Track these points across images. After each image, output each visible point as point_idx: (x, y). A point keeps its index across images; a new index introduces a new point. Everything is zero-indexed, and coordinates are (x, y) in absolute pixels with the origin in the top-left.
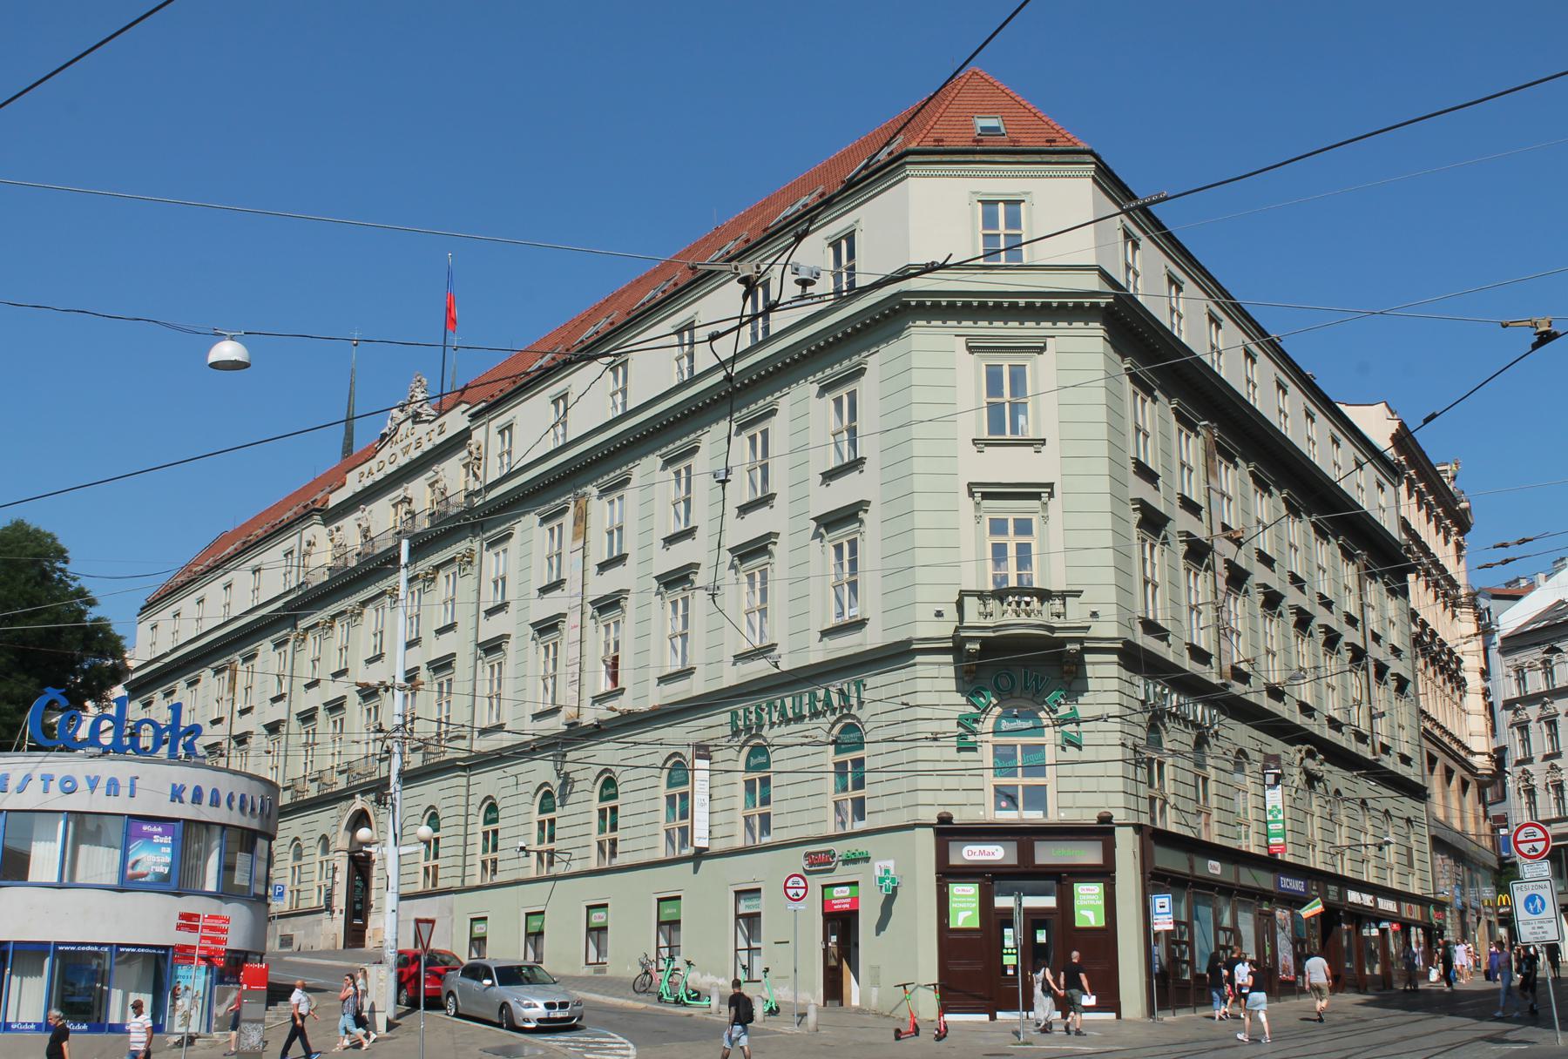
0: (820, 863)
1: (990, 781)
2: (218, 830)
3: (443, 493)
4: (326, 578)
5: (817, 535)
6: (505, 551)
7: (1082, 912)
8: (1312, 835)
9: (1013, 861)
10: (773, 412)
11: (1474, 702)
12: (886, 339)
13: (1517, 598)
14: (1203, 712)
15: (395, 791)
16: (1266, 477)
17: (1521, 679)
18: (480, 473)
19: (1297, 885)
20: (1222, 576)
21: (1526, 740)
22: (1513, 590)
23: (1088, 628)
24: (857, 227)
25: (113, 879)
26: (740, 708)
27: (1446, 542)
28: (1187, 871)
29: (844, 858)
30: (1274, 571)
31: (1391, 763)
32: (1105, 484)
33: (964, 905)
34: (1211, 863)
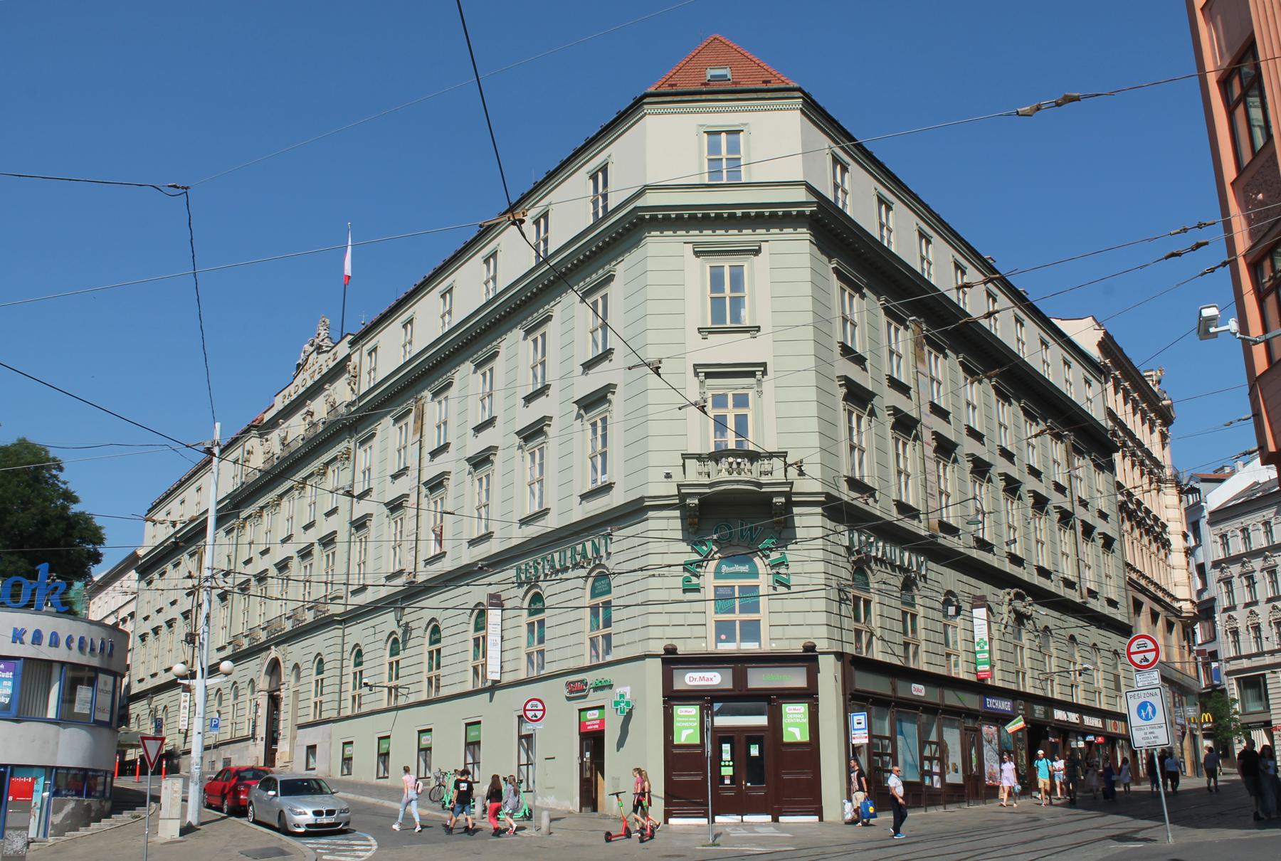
0: (577, 691)
3: (332, 406)
5: (579, 416)
6: (370, 447)
7: (789, 729)
8: (1022, 664)
9: (729, 685)
10: (549, 318)
11: (1177, 558)
12: (629, 250)
13: (1221, 481)
14: (910, 558)
15: (204, 632)
16: (975, 367)
17: (1225, 544)
19: (1004, 705)
20: (929, 445)
21: (1230, 592)
22: (1218, 475)
24: (609, 160)
26: (522, 563)
27: (1152, 431)
28: (890, 693)
29: (594, 686)
30: (983, 444)
31: (1098, 606)
33: (687, 724)
34: (914, 686)
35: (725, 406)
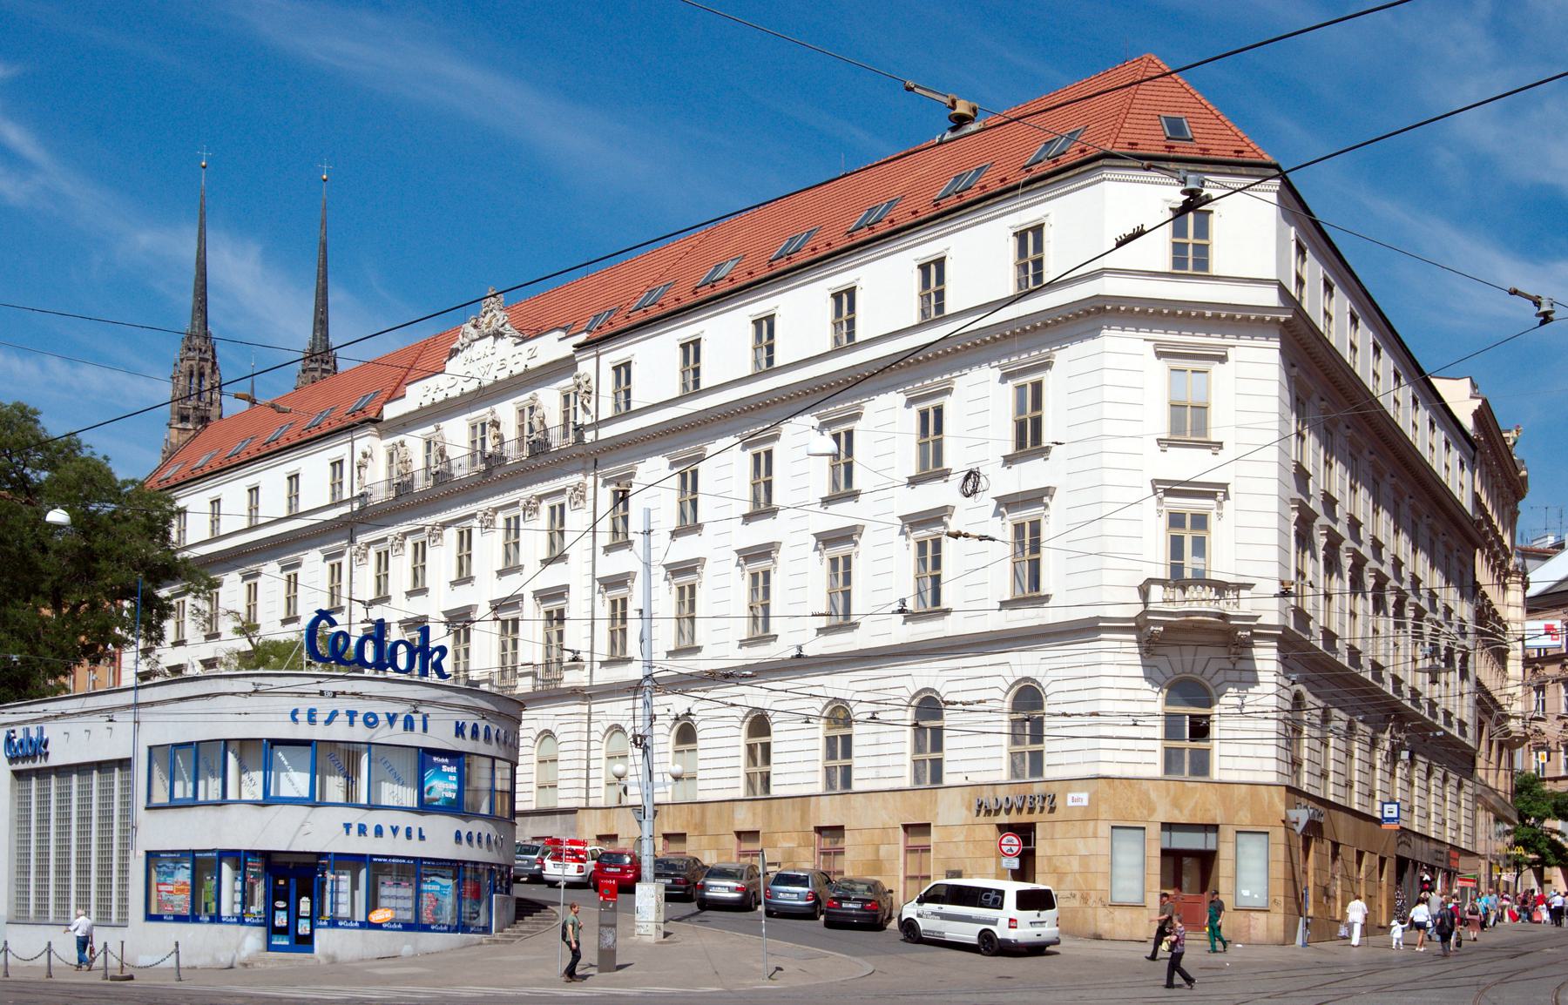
18: (592, 407)
23: (1256, 618)
35: (1183, 526)
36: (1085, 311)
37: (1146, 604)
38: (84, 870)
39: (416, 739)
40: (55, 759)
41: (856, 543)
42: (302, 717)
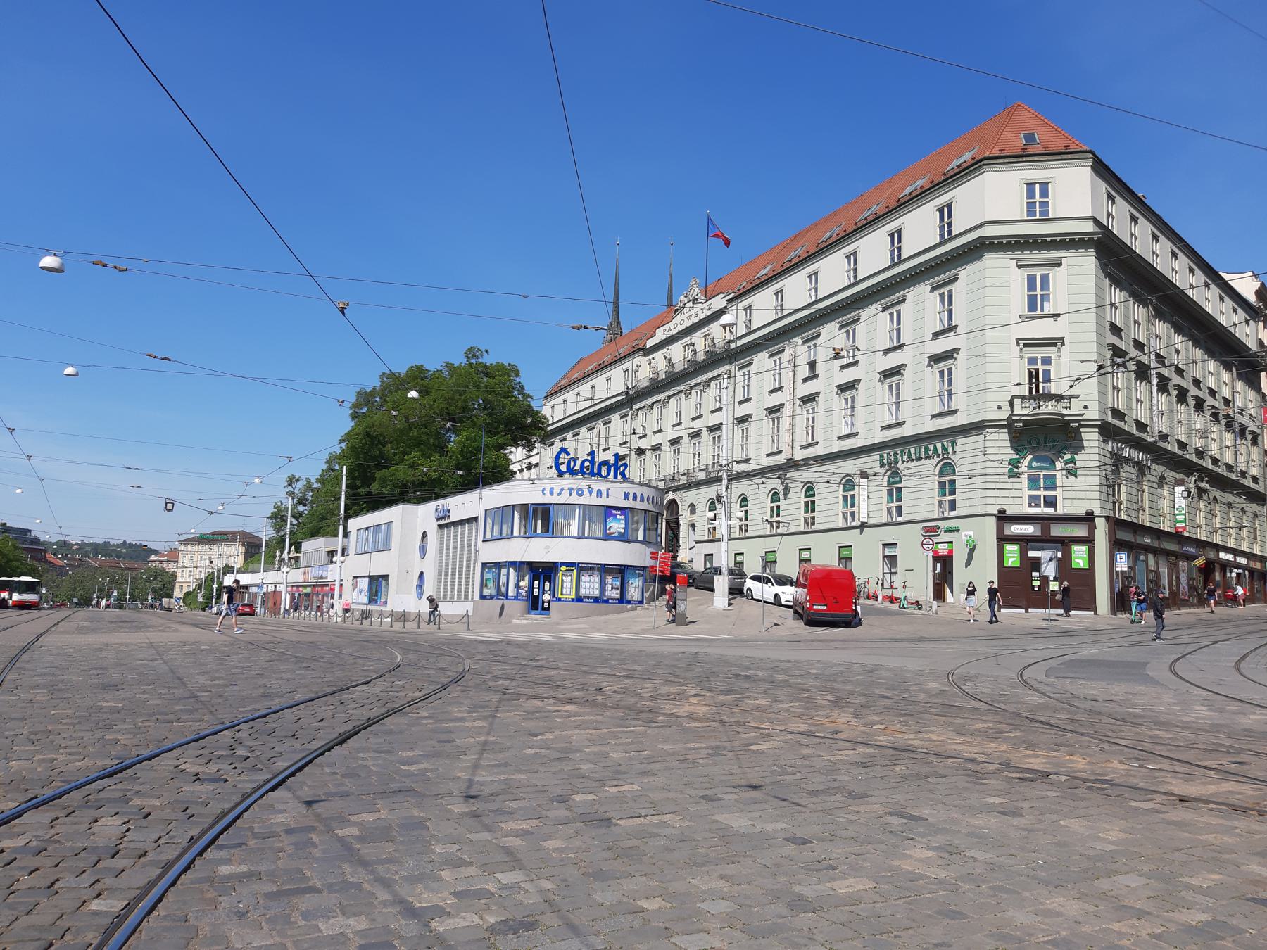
0: (931, 532)
1: (1026, 493)
2: (518, 508)
4: (648, 384)
5: (929, 365)
10: (904, 301)
12: (972, 261)
18: (734, 331)
19: (1192, 550)
23: (1083, 415)
24: (954, 200)
25: (600, 535)
26: (885, 453)
31: (1247, 482)
32: (1093, 337)
36: (974, 246)
37: (1012, 411)
38: (460, 574)
39: (603, 501)
40: (452, 519)
41: (857, 389)
42: (547, 492)
